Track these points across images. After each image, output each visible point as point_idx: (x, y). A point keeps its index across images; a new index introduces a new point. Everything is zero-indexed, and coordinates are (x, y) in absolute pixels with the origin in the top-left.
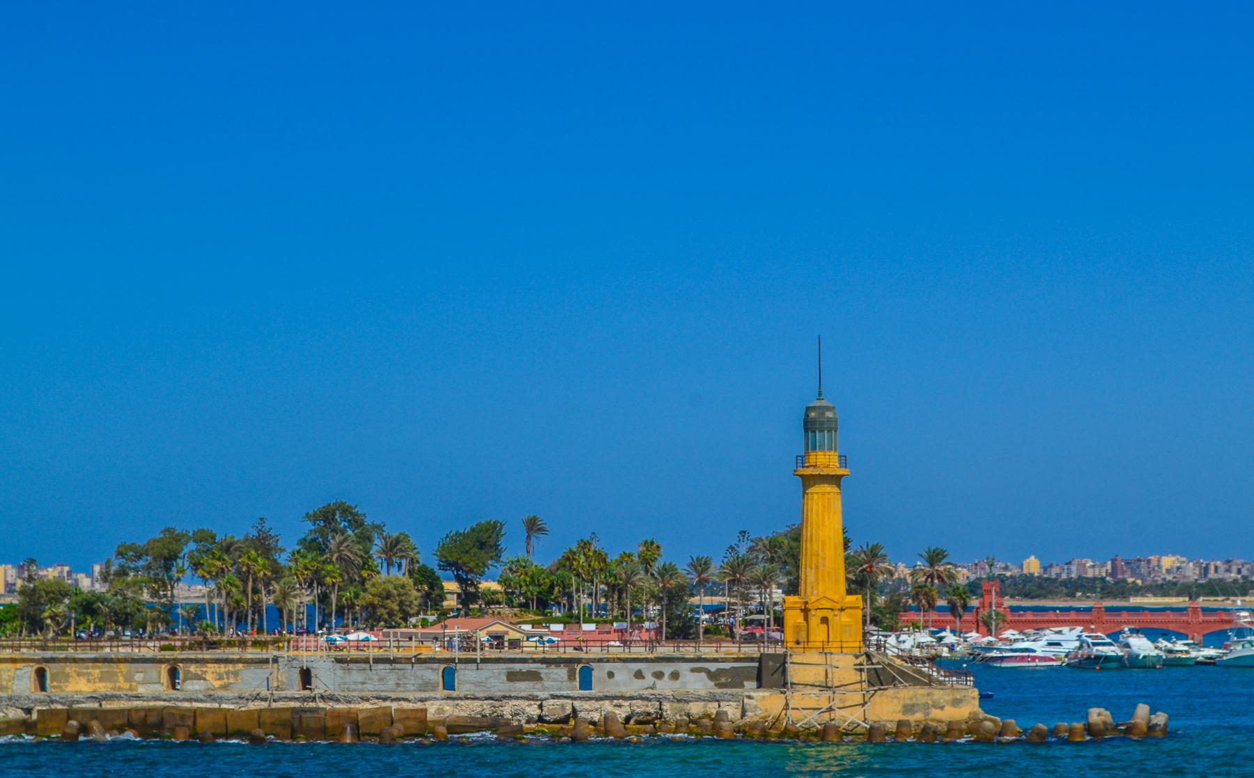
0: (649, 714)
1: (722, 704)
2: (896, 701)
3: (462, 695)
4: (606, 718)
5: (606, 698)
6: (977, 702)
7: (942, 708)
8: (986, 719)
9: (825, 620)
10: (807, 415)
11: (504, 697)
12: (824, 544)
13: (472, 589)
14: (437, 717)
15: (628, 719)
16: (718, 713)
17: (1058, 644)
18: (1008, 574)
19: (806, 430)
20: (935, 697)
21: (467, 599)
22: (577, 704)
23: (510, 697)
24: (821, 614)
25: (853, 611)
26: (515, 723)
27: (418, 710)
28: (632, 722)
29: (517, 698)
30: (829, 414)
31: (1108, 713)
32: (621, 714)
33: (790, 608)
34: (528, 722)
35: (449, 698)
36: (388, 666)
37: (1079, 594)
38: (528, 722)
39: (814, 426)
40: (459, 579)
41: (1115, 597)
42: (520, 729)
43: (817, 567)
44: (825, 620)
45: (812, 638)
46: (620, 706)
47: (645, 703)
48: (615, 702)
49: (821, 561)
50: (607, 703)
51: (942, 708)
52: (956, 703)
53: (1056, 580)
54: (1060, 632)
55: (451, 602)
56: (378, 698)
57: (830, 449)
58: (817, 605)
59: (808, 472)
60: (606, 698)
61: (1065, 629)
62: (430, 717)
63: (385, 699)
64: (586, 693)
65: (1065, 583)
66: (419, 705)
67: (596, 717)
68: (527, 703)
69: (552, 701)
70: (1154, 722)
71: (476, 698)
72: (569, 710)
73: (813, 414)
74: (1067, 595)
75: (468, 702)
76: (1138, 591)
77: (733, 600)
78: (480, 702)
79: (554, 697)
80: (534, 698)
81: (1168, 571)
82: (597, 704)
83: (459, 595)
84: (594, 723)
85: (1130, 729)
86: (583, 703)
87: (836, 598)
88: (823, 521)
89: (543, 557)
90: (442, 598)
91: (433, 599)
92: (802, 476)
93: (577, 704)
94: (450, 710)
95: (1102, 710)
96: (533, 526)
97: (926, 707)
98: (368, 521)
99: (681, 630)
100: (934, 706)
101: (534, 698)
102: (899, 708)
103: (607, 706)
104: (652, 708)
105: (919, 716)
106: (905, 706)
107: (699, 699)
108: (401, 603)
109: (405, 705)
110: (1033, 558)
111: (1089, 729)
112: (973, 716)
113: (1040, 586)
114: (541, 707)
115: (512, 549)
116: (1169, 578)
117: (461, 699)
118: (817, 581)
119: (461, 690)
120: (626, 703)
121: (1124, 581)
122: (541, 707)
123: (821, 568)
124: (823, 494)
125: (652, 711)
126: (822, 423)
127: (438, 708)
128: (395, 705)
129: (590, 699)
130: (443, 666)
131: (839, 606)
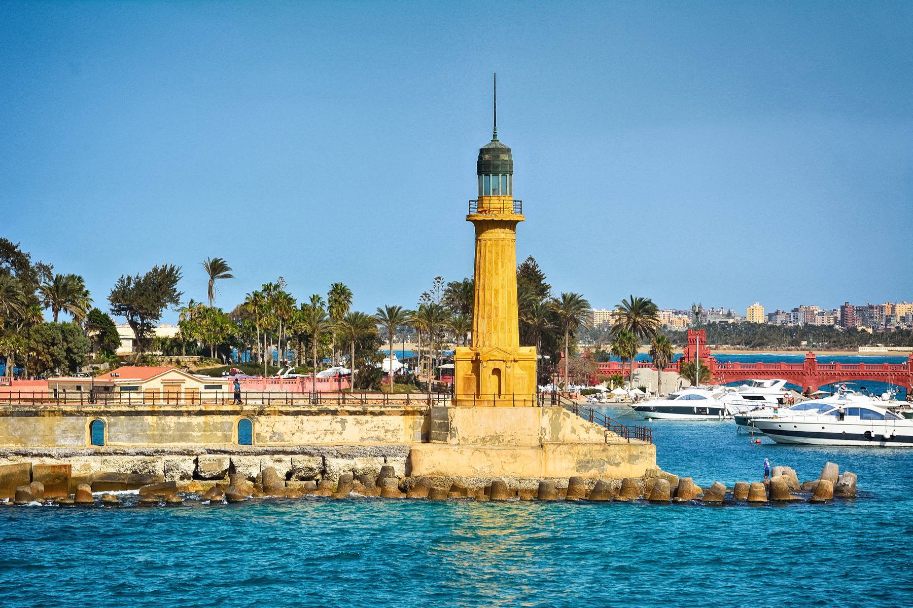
0: (311, 469)
1: (388, 459)
2: (569, 457)
3: (111, 450)
4: (263, 473)
5: (267, 452)
6: (654, 459)
7: (618, 465)
8: (663, 477)
9: (497, 372)
10: (480, 158)
11: (157, 452)
12: (497, 291)
13: (148, 335)
14: (83, 474)
15: (289, 476)
16: (384, 469)
17: (761, 398)
18: (731, 321)
19: (480, 173)
20: (611, 453)
21: (141, 343)
22: (235, 458)
23: (163, 452)
24: (492, 365)
25: (527, 363)
26: (169, 480)
27: (60, 467)
28: (294, 478)
29: (170, 453)
30: (504, 157)
31: (794, 471)
32: (282, 469)
33: (461, 360)
34: (182, 478)
35: (96, 453)
36: (329, 417)
37: (804, 343)
38: (182, 478)
39: (491, 163)
40: (133, 324)
41: (842, 347)
42: (171, 487)
43: (490, 317)
44: (497, 372)
45: (483, 390)
46: (280, 461)
47: (307, 457)
48: (276, 456)
49: (494, 311)
50: (267, 457)
51: (618, 465)
52: (632, 459)
53: (779, 328)
54: (760, 385)
55: (125, 348)
56: (17, 454)
57: (505, 193)
58: (487, 357)
59: (481, 217)
60: (267, 452)
61: (767, 383)
62: (74, 473)
63: (25, 455)
64: (245, 448)
65: (791, 332)
66: (64, 462)
67: (255, 473)
68: (181, 457)
69: (208, 456)
70: (842, 482)
71: (125, 454)
72: (226, 466)
73: (487, 156)
74: (791, 344)
75: (116, 457)
76: (867, 340)
77: (425, 349)
78: (131, 457)
79: (210, 452)
80: (189, 453)
81: (903, 319)
82: (256, 459)
83: (135, 342)
84: (252, 479)
85: (816, 490)
86: (242, 458)
87: (509, 349)
88: (497, 269)
89: (229, 299)
90: (117, 343)
91: (107, 340)
92: (475, 222)
93: (235, 458)
94: (97, 467)
95: (788, 469)
96: (217, 268)
97: (601, 463)
98: (33, 263)
99: (370, 380)
100: (608, 462)
101: (189, 453)
102: (574, 464)
103: (268, 461)
104: (315, 463)
105: (593, 472)
106: (579, 462)
107: (365, 454)
108: (69, 350)
109: (48, 461)
110: (757, 304)
111: (771, 489)
112: (650, 474)
113: (763, 335)
114: (196, 461)
115: (192, 288)
116: (904, 327)
117: (110, 454)
118: (489, 331)
119: (110, 444)
120: (287, 458)
121: (855, 329)
122: (196, 461)
123: (493, 316)
124: (497, 240)
125: (314, 466)
126: (497, 166)
127: (87, 466)
128: (35, 462)
129: (248, 453)
130: (90, 419)
131: (511, 358)
